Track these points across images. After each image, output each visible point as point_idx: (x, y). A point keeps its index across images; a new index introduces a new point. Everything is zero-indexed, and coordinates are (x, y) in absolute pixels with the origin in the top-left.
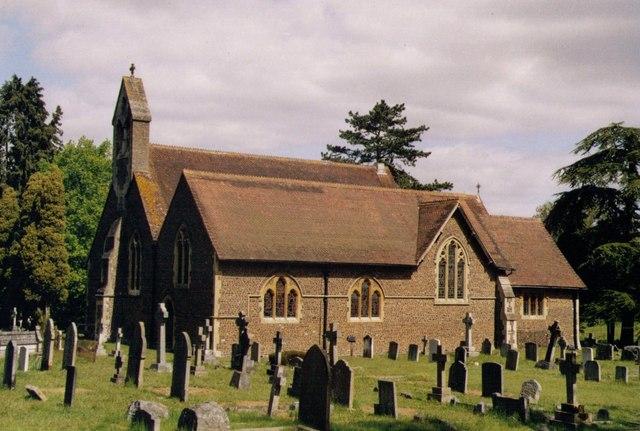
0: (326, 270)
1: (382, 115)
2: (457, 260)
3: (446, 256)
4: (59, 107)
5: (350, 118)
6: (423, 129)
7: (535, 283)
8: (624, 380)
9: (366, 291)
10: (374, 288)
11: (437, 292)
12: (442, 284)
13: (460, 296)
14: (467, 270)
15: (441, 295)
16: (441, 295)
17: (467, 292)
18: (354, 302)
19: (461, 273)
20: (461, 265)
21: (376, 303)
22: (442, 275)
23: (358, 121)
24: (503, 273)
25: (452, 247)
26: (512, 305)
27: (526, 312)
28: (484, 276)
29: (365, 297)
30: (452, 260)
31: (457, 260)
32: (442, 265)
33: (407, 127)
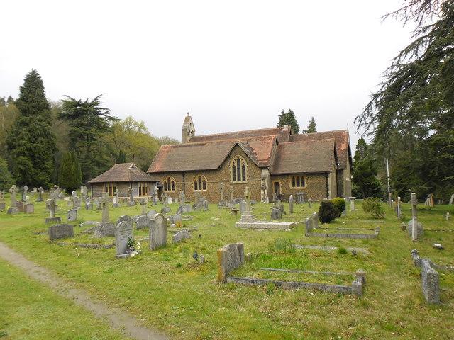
0: (183, 173)
3: (236, 165)
4: (188, 119)
9: (200, 179)
11: (232, 178)
12: (234, 176)
14: (246, 169)
15: (234, 180)
16: (234, 180)
18: (196, 184)
19: (244, 171)
20: (244, 167)
22: (234, 172)
27: (293, 185)
28: (255, 170)
29: (200, 183)
30: (239, 165)
32: (234, 167)
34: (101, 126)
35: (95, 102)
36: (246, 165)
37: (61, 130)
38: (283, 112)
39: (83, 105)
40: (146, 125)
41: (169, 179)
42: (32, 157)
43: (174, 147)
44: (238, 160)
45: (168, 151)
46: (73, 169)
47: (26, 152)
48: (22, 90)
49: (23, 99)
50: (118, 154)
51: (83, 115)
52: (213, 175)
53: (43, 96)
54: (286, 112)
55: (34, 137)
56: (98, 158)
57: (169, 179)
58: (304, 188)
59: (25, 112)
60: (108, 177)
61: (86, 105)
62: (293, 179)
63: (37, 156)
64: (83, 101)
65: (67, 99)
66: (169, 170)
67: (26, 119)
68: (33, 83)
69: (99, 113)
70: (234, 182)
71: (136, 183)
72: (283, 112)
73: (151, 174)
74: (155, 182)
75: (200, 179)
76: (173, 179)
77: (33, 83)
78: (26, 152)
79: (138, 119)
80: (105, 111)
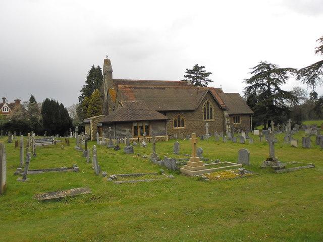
1: (197, 68)
2: (210, 107)
4: (210, 73)
5: (187, 71)
6: (210, 73)
7: (166, 109)
8: (79, 127)
9: (179, 119)
10: (181, 118)
12: (205, 115)
13: (211, 118)
15: (205, 119)
17: (213, 117)
18: (175, 122)
19: (211, 111)
20: (211, 109)
21: (183, 122)
22: (205, 113)
23: (189, 72)
24: (225, 110)
25: (208, 103)
26: (227, 120)
29: (179, 121)
30: (208, 107)
31: (210, 107)
32: (205, 109)
33: (206, 72)
36: (213, 108)
38: (93, 67)
44: (208, 103)
52: (190, 114)
54: (96, 67)
58: (240, 123)
62: (234, 118)
66: (172, 109)
70: (205, 120)
72: (93, 67)
75: (179, 119)
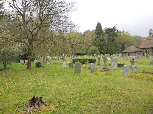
20: (148, 51)
34: (117, 35)
35: (114, 28)
37: (106, 37)
39: (111, 29)
40: (129, 32)
41: (147, 50)
42: (100, 46)
43: (147, 40)
45: (145, 42)
46: (112, 49)
47: (99, 45)
48: (96, 28)
49: (97, 30)
50: (122, 43)
51: (111, 32)
53: (101, 29)
55: (100, 40)
56: (116, 45)
57: (147, 50)
59: (97, 34)
60: (139, 50)
61: (111, 29)
63: (101, 46)
64: (111, 28)
65: (105, 28)
67: (98, 36)
68: (99, 25)
69: (115, 31)
71: (137, 52)
73: (140, 49)
74: (142, 51)
76: (148, 50)
77: (99, 25)
78: (99, 45)
79: (126, 31)
80: (117, 30)
